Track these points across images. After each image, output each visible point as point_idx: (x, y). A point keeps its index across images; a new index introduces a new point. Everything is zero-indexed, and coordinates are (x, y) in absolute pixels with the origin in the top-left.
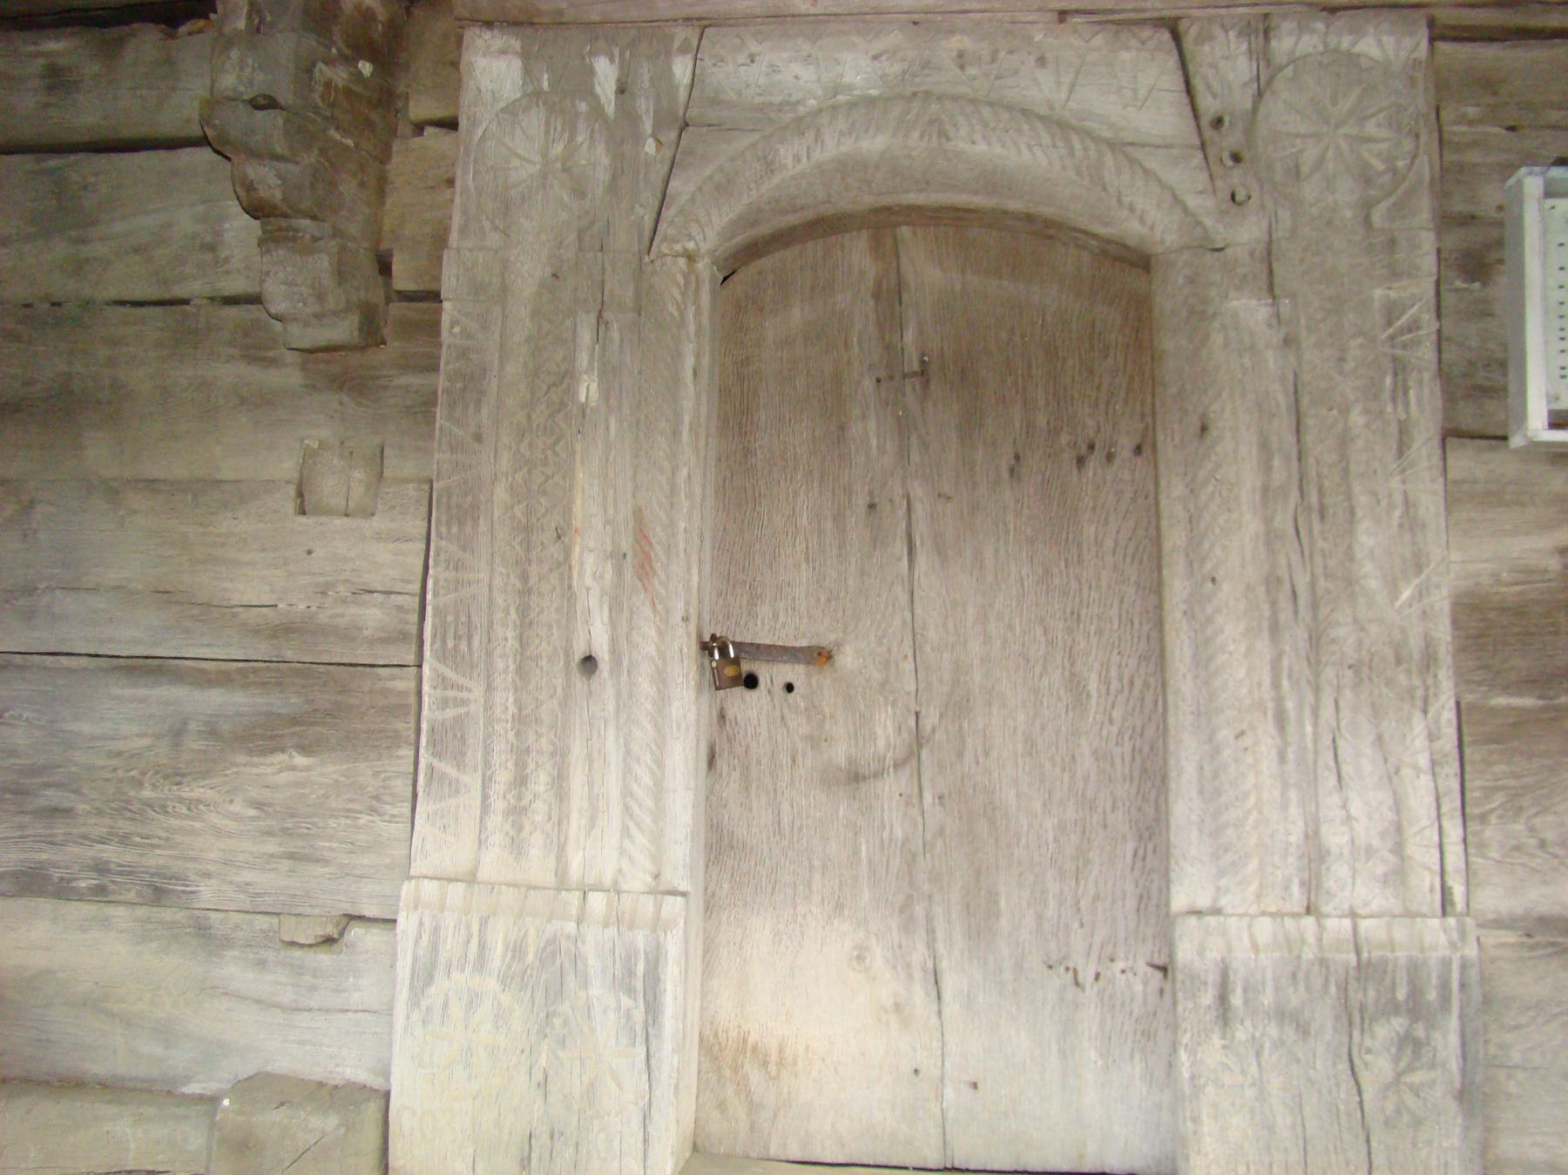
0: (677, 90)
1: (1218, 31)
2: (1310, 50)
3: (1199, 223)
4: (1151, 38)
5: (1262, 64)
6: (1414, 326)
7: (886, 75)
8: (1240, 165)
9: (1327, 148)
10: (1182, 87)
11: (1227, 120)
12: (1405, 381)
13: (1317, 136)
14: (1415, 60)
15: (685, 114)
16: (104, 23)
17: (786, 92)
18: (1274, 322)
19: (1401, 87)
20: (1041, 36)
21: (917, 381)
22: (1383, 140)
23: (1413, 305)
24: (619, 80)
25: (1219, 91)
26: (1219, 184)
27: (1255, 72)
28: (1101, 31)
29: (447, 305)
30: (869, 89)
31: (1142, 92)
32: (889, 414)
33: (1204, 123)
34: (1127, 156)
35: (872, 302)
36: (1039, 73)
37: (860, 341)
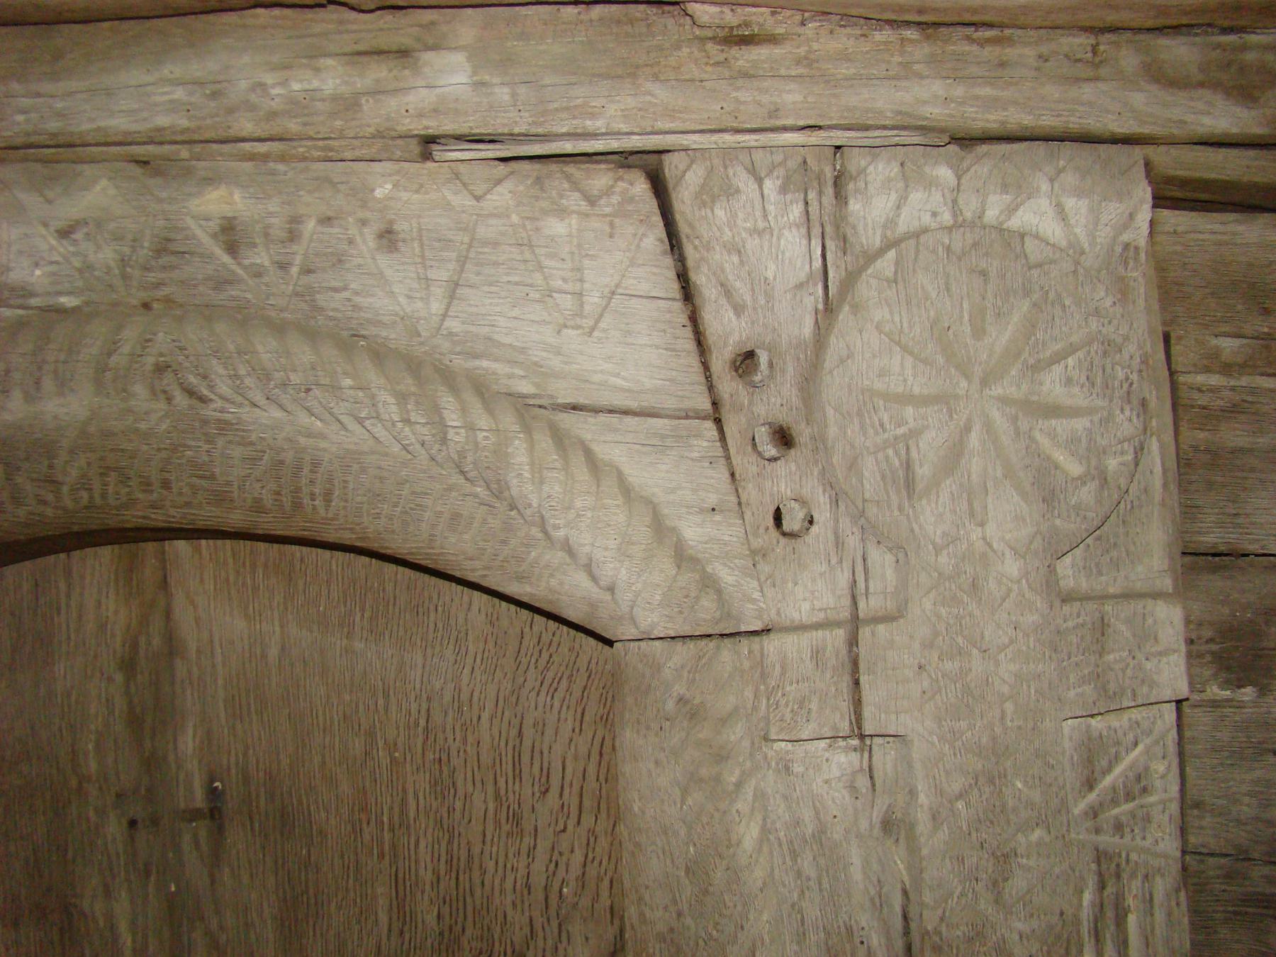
2: (927, 219)
3: (709, 583)
4: (608, 192)
5: (830, 245)
6: (1138, 785)
7: (90, 267)
8: (792, 451)
9: (967, 429)
10: (674, 288)
11: (763, 358)
13: (943, 400)
14: (1126, 246)
16: (46, 162)
18: (863, 782)
19: (1108, 302)
20: (389, 186)
21: (203, 828)
22: (1075, 412)
27: (818, 263)
30: (60, 293)
31: (593, 300)
32: (151, 889)
33: (719, 363)
34: (560, 438)
35: (119, 678)
37: (98, 747)
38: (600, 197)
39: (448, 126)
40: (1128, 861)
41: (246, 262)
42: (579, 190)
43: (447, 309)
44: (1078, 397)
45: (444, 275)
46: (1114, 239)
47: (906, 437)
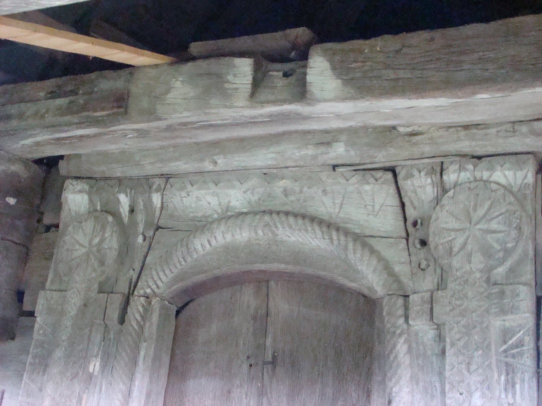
0: (155, 211)
1: (416, 173)
6: (520, 344)
12: (513, 378)
14: (526, 184)
15: (158, 222)
17: (204, 210)
18: (438, 339)
21: (270, 367)
22: (500, 232)
23: (520, 331)
24: (130, 206)
25: (417, 205)
26: (413, 258)
28: (356, 174)
29: (38, 319)
31: (377, 207)
35: (252, 322)
36: (324, 199)
38: (379, 179)
39: (340, 162)
40: (516, 367)
41: (290, 199)
42: (373, 178)
43: (340, 211)
44: (502, 228)
45: (339, 202)
46: (522, 182)
47: (451, 241)
